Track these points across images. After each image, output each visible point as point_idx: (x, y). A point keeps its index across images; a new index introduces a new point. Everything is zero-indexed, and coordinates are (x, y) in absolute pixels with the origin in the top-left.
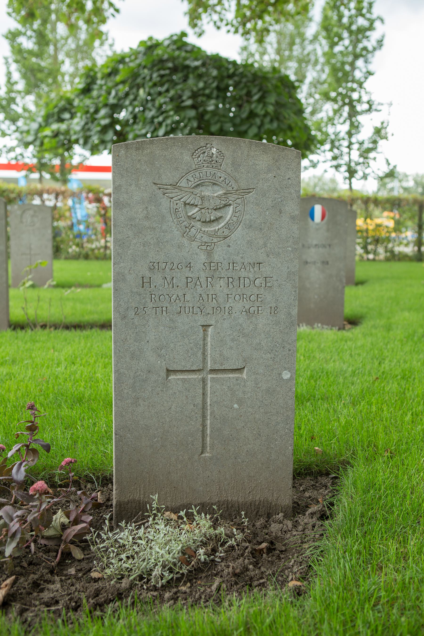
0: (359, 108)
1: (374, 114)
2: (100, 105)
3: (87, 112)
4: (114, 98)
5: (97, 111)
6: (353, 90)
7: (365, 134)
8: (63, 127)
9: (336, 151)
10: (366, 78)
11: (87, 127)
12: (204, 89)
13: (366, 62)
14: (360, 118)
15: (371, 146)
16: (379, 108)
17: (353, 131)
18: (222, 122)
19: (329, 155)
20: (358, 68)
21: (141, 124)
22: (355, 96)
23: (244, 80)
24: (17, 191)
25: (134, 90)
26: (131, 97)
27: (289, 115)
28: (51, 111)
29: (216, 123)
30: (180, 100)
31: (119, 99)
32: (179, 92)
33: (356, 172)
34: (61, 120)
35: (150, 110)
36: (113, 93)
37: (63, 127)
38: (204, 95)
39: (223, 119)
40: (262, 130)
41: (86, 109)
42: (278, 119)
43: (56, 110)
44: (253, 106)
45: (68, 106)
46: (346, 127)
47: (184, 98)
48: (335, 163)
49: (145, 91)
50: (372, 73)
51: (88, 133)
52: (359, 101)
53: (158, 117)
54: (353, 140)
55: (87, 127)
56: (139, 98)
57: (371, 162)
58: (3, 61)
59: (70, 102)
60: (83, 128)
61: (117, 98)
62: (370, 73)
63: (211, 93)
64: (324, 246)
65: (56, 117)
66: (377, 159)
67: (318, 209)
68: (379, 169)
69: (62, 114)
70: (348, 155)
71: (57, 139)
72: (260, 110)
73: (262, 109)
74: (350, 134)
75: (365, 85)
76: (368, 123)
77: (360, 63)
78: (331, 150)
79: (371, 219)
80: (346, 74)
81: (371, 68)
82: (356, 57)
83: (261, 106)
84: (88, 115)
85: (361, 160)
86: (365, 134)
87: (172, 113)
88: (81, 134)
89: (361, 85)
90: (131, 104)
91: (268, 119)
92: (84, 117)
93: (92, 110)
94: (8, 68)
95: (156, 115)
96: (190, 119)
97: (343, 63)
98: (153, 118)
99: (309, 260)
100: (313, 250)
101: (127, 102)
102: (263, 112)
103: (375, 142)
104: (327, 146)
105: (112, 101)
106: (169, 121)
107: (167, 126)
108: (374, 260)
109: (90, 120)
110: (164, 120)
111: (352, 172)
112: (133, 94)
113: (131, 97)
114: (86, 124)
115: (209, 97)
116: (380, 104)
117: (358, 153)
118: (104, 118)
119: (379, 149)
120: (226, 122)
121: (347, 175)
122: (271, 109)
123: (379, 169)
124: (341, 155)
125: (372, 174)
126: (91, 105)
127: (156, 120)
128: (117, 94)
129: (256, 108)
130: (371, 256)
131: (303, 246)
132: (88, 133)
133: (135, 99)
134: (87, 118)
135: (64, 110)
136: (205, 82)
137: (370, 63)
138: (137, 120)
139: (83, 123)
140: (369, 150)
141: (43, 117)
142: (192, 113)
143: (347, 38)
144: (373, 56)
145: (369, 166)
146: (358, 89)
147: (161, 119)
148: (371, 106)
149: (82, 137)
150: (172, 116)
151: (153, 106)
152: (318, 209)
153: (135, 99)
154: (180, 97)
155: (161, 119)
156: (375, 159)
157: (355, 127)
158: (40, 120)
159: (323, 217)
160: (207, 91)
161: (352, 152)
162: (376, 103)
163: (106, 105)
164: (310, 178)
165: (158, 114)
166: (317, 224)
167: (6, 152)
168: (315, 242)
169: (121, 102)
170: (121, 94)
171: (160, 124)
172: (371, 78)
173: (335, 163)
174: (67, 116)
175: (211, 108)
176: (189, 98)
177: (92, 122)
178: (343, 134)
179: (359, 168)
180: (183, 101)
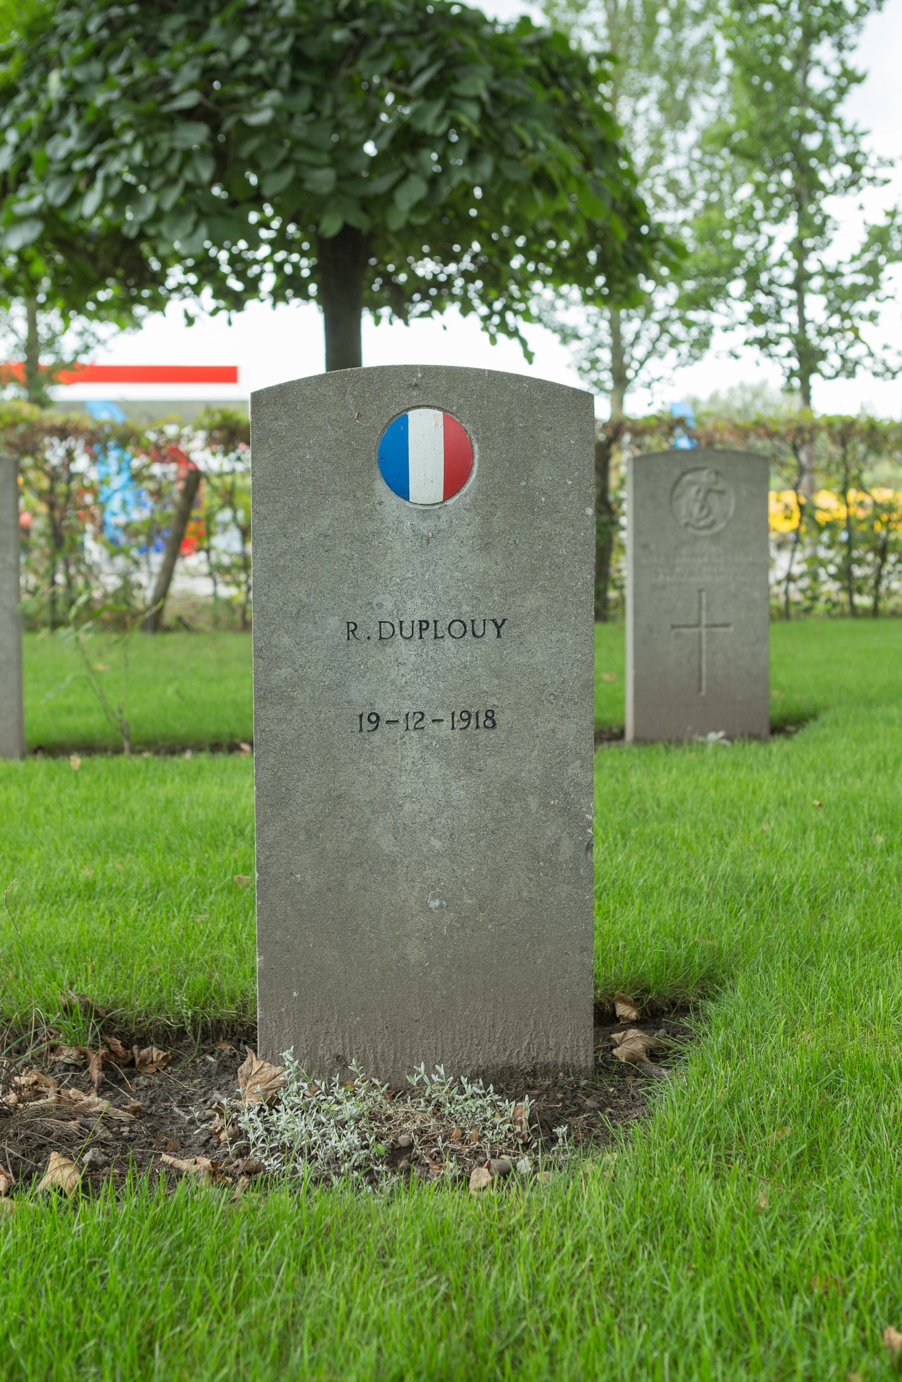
0: (824, 177)
1: (868, 193)
6: (807, 127)
7: (842, 248)
9: (760, 297)
10: (842, 92)
12: (249, 58)
13: (840, 47)
14: (829, 204)
15: (861, 279)
16: (882, 173)
17: (809, 243)
19: (742, 309)
20: (818, 63)
22: (812, 142)
23: (387, 28)
25: (34, 79)
27: (535, 136)
30: (159, 96)
32: (165, 73)
33: (823, 355)
39: (302, 155)
42: (498, 149)
46: (788, 230)
47: (176, 88)
48: (759, 332)
50: (859, 72)
52: (825, 152)
54: (811, 265)
57: (865, 328)
62: (850, 78)
63: (274, 73)
64: (469, 630)
66: (881, 319)
67: (426, 432)
68: (886, 347)
70: (794, 310)
73: (440, 118)
74: (799, 250)
75: (839, 111)
76: (849, 218)
77: (824, 50)
78: (748, 294)
79: (861, 488)
80: (783, 81)
81: (854, 61)
82: (811, 35)
83: (437, 108)
85: (835, 322)
86: (842, 248)
89: (826, 111)
97: (775, 52)
98: (71, 156)
99: (385, 709)
100: (407, 651)
103: (873, 270)
104: (737, 287)
107: (108, 179)
108: (874, 612)
110: (99, 165)
111: (808, 358)
113: (21, 99)
115: (264, 84)
116: (881, 162)
117: (822, 300)
119: (886, 288)
121: (795, 363)
122: (470, 114)
123: (886, 347)
124: (779, 308)
125: (868, 362)
127: (78, 165)
130: (864, 601)
131: (352, 629)
133: (32, 102)
136: (255, 40)
137: (852, 48)
140: (858, 292)
142: (195, 135)
144: (860, 28)
145: (857, 337)
146: (821, 124)
147: (91, 160)
148: (856, 168)
150: (129, 147)
152: (426, 432)
156: (873, 317)
157: (815, 228)
159: (454, 480)
160: (260, 67)
161: (809, 299)
162: (873, 160)
164: (731, 391)
166: (426, 511)
168: (416, 611)
171: (90, 174)
172: (855, 89)
173: (759, 332)
175: (261, 117)
176: (191, 86)
178: (778, 250)
179: (827, 344)
180: (173, 97)
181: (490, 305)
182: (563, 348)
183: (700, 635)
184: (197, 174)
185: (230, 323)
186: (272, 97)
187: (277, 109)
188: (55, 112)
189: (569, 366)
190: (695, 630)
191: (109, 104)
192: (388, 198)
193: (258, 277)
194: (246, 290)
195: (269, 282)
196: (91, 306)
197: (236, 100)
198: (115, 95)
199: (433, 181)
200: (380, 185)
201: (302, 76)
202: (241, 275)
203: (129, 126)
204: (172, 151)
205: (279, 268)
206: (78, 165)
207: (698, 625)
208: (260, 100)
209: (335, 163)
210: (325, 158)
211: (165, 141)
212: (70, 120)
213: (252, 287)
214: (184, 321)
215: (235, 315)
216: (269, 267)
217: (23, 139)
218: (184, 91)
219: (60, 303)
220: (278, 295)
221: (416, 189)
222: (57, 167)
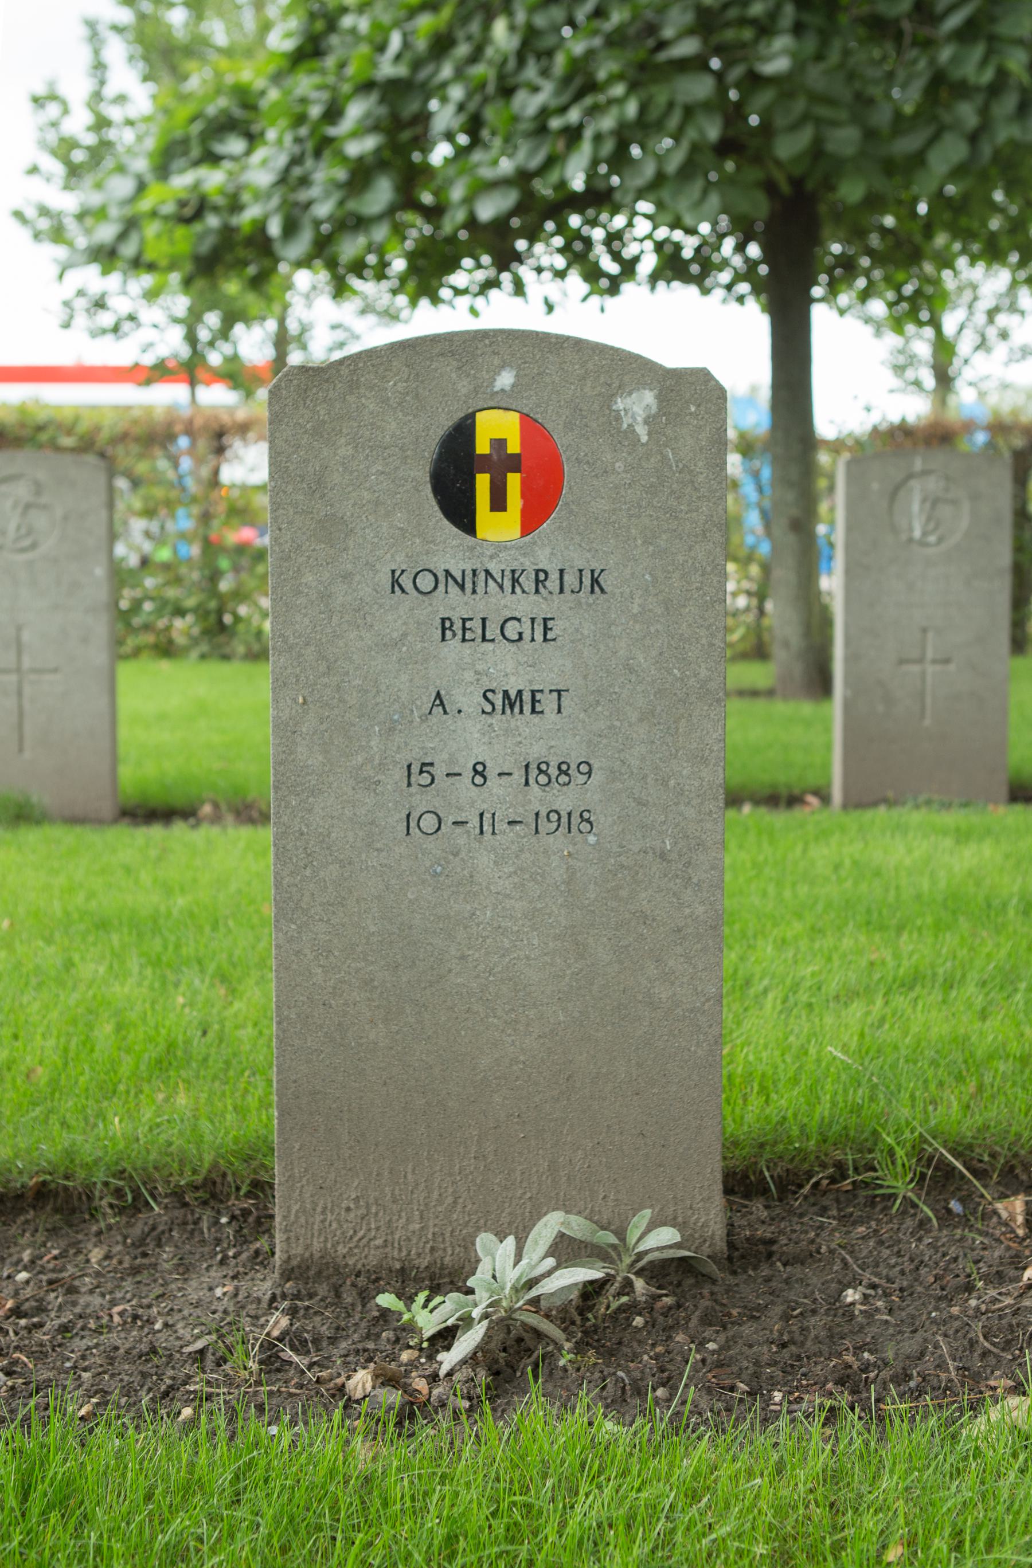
2: (346, 88)
3: (300, 119)
4: (398, 58)
5: (333, 113)
8: (214, 180)
11: (297, 171)
18: (819, 122)
21: (497, 142)
24: (83, 428)
25: (475, 27)
26: (463, 50)
28: (178, 134)
29: (795, 127)
30: (651, 43)
31: (417, 65)
34: (213, 159)
35: (535, 89)
36: (395, 41)
37: (214, 180)
38: (743, 22)
39: (823, 111)
40: (986, 151)
41: (298, 109)
43: (196, 128)
44: (946, 54)
45: (238, 113)
47: (668, 32)
49: (512, 28)
51: (303, 196)
53: (563, 110)
55: (297, 171)
56: (489, 52)
58: (83, 31)
59: (247, 100)
60: (283, 179)
61: (408, 56)
65: (196, 152)
69: (221, 141)
71: (197, 227)
72: (972, 67)
73: (984, 62)
83: (978, 51)
84: (303, 131)
87: (618, 90)
88: (275, 201)
90: (459, 74)
91: (1009, 103)
92: (288, 139)
93: (315, 111)
94: (97, 52)
95: (554, 103)
96: (689, 111)
98: (544, 114)
101: (447, 71)
102: (988, 76)
105: (387, 69)
106: (607, 123)
107: (598, 138)
109: (309, 146)
112: (469, 38)
113: (463, 50)
114: (296, 161)
118: (355, 134)
120: (834, 124)
126: (315, 95)
127: (555, 123)
128: (406, 45)
129: (955, 60)
132: (303, 196)
133: (475, 57)
134: (298, 140)
135: (225, 125)
138: (485, 134)
139: (282, 160)
141: (150, 155)
143: (751, 293)
147: (574, 115)
149: (279, 209)
150: (620, 101)
151: (545, 73)
153: (475, 57)
154: (652, 29)
155: (574, 115)
158: (141, 165)
163: (367, 86)
165: (564, 99)
167: (88, 311)
169: (423, 74)
170: (421, 44)
174: (235, 145)
177: (318, 154)
180: (662, 45)
181: (898, 289)
182: (875, 341)
183: (923, 674)
184: (702, 133)
185: (602, 310)
186: (782, 42)
187: (794, 55)
188: (512, 64)
189: (883, 363)
190: (915, 668)
191: (590, 53)
192: (918, 160)
193: (636, 259)
194: (622, 273)
195: (648, 263)
196: (445, 293)
197: (743, 45)
198: (597, 42)
199: (973, 139)
200: (906, 145)
201: (808, 18)
202: (616, 256)
203: (619, 77)
204: (671, 105)
205: (659, 246)
206: (555, 123)
207: (921, 660)
208: (769, 46)
209: (856, 119)
210: (843, 115)
211: (661, 96)
212: (531, 72)
213: (629, 267)
214: (543, 308)
215: (610, 302)
216: (649, 245)
217: (469, 95)
218: (681, 36)
219: (411, 285)
220: (654, 278)
221: (952, 151)
222: (524, 126)
